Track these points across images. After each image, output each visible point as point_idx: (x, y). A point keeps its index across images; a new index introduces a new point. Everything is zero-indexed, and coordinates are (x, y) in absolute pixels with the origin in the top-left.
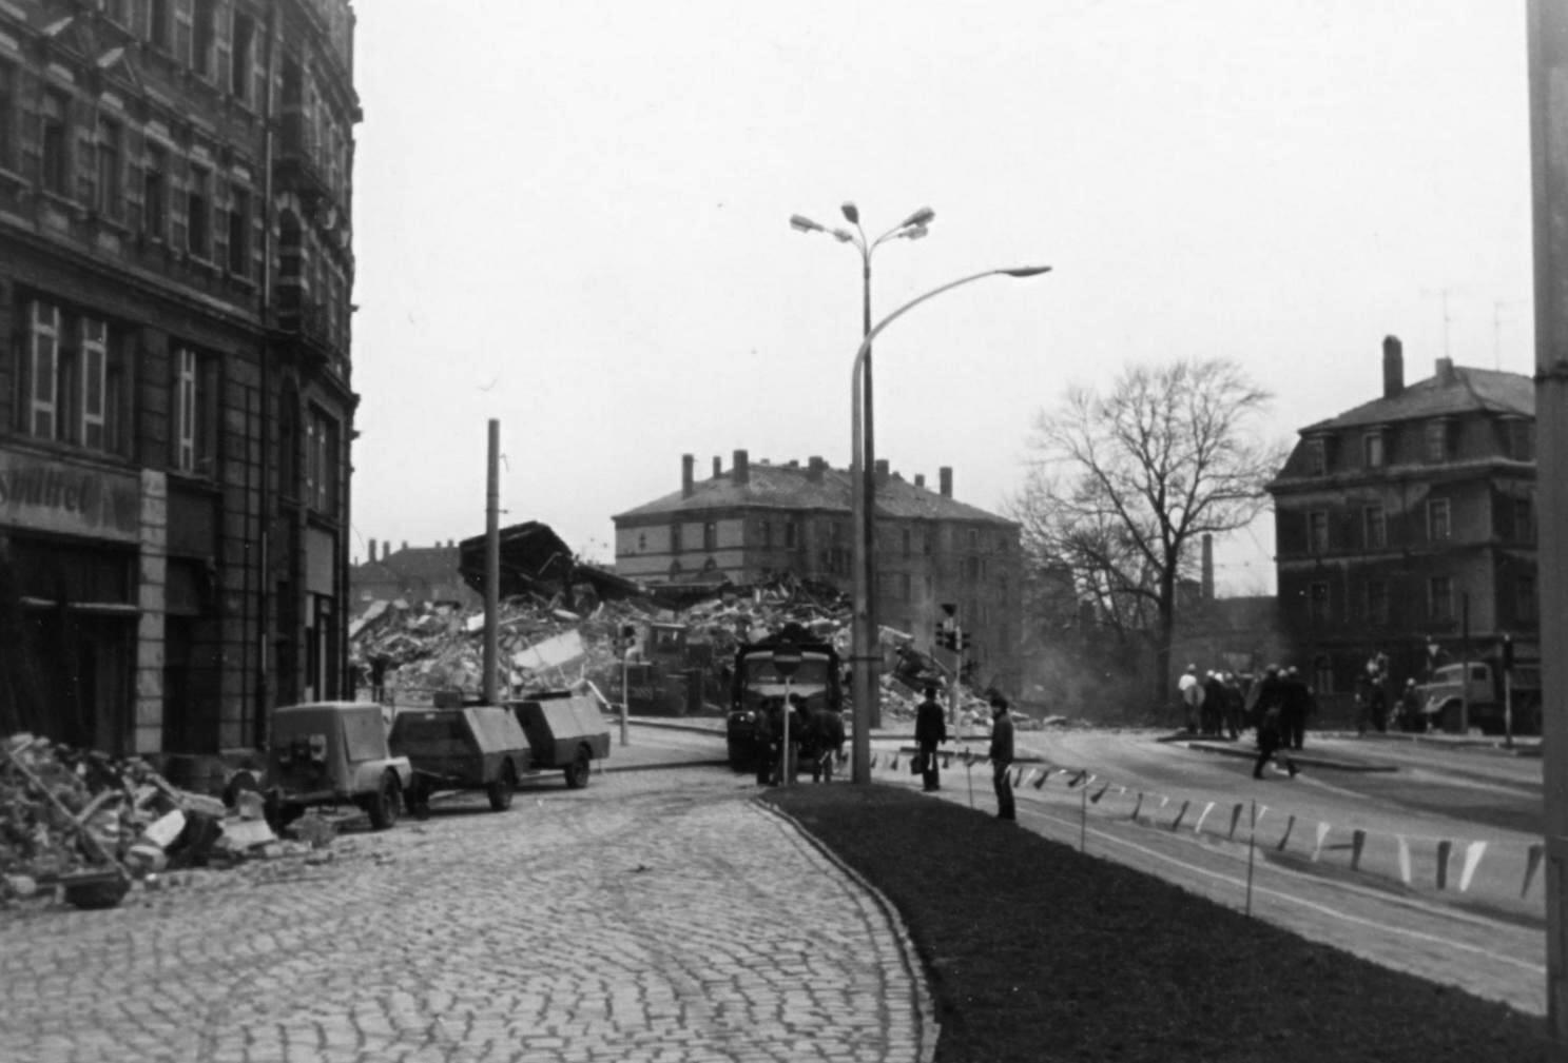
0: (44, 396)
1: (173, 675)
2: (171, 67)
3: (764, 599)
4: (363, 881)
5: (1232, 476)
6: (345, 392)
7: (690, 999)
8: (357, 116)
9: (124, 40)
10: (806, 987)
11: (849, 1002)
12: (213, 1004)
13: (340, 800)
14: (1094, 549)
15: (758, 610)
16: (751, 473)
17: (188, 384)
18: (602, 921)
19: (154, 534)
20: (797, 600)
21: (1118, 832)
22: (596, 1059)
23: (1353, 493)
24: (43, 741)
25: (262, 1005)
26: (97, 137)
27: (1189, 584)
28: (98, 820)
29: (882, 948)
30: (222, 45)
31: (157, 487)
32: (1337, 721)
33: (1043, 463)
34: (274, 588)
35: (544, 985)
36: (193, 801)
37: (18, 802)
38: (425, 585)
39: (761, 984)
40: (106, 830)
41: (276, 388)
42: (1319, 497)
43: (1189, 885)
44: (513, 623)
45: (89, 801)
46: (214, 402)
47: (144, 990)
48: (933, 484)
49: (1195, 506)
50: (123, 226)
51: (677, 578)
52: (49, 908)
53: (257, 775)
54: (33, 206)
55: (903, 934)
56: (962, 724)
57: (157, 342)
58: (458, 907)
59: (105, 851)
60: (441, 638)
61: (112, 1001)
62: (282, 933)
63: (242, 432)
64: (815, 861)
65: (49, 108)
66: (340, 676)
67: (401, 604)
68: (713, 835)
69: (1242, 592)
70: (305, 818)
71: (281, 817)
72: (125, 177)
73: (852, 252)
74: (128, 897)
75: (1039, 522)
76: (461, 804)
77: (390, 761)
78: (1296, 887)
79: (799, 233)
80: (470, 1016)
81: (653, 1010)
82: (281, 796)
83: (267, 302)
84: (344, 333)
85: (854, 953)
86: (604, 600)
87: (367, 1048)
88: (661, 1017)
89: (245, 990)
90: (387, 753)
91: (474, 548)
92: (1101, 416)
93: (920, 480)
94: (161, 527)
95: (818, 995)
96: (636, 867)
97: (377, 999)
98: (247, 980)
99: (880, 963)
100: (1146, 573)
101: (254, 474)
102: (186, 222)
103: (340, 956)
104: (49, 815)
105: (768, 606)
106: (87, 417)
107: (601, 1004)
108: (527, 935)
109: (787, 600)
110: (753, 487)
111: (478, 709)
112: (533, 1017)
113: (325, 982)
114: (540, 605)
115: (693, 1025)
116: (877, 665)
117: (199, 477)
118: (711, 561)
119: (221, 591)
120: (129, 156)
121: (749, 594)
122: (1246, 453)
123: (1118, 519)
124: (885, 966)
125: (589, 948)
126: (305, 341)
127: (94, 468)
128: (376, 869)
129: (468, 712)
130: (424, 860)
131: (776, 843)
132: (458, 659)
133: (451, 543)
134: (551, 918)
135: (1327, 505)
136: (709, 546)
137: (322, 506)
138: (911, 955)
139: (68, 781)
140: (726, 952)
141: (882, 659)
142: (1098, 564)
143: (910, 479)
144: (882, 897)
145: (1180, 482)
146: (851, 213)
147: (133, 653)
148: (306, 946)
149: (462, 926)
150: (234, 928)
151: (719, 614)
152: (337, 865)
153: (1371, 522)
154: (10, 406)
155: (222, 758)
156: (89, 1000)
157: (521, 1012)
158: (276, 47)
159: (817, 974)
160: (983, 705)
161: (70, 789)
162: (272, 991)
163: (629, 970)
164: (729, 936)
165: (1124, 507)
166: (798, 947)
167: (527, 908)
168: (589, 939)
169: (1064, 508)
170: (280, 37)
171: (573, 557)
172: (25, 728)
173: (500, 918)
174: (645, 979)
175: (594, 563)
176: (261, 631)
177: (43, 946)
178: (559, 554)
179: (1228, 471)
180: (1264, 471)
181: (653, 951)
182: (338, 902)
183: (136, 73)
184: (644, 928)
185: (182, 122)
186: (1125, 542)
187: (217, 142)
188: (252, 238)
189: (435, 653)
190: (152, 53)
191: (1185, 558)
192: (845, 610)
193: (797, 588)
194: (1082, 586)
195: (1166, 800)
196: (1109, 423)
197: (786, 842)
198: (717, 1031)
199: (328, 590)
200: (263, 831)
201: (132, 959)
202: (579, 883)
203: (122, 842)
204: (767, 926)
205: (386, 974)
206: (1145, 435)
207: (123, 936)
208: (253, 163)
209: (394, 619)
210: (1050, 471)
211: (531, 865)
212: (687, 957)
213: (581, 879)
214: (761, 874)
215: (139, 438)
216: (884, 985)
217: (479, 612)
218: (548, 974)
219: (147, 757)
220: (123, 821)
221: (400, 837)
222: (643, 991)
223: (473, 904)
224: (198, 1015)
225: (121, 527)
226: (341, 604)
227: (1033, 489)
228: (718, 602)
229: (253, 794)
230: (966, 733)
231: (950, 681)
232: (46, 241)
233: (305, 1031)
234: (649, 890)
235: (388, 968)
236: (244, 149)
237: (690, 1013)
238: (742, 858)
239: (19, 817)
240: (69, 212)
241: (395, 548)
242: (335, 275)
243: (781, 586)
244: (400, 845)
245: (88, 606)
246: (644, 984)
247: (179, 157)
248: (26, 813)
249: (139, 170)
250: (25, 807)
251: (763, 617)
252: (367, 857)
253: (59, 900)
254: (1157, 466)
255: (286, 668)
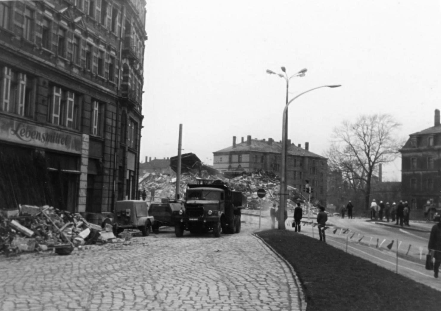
0: (56, 113)
1: (89, 191)
2: (94, 22)
3: (255, 176)
4: (139, 250)
5: (389, 147)
6: (140, 115)
7: (232, 290)
8: (146, 38)
9: (81, 14)
10: (266, 289)
11: (279, 294)
12: (93, 285)
13: (134, 227)
14: (349, 166)
15: (253, 180)
16: (252, 142)
17: (96, 111)
18: (207, 266)
19: (85, 151)
20: (264, 177)
21: (355, 246)
22: (204, 308)
23: (424, 153)
24: (52, 208)
25: (108, 285)
26: (74, 41)
27: (375, 177)
28: (66, 230)
29: (288, 278)
30: (109, 17)
31: (86, 139)
32: (418, 218)
33: (335, 142)
34: (118, 168)
35: (189, 284)
36: (93, 226)
37: (44, 224)
38: (161, 169)
39: (253, 287)
40: (68, 233)
41: (120, 113)
42: (415, 154)
43: (379, 264)
44: (184, 181)
45: (64, 225)
46: (103, 116)
47: (75, 280)
48: (303, 147)
49: (378, 155)
50: (80, 66)
51: (230, 170)
52: (51, 255)
53: (111, 219)
54: (55, 60)
55: (295, 274)
56: (310, 214)
57: (88, 99)
58: (165, 260)
59: (68, 239)
60: (164, 184)
61: (65, 282)
62: (115, 265)
63: (111, 125)
64: (268, 251)
65: (60, 33)
66: (136, 193)
67: (154, 174)
68: (239, 242)
69: (391, 180)
70: (124, 232)
71: (117, 232)
72: (81, 52)
73: (283, 80)
74: (73, 252)
75: (333, 158)
76: (168, 230)
77: (148, 217)
78: (410, 266)
79: (268, 75)
80: (167, 292)
81: (221, 293)
82: (118, 226)
83: (119, 89)
84: (140, 98)
85: (280, 279)
86: (210, 175)
87: (137, 301)
88: (223, 296)
89: (103, 281)
90: (148, 215)
91: (174, 159)
92: (352, 129)
93: (299, 145)
94: (87, 150)
95: (270, 291)
96: (217, 250)
97: (141, 285)
98: (104, 278)
99: (288, 282)
100: (363, 174)
101: (114, 136)
102: (97, 66)
103: (131, 272)
104: (52, 229)
105: (256, 178)
106: (68, 119)
107: (206, 291)
108: (185, 269)
109: (261, 177)
110: (253, 146)
111: (173, 204)
112: (186, 293)
113: (126, 280)
114: (192, 176)
115: (232, 299)
116: (287, 196)
117: (98, 136)
118: (240, 166)
119: (103, 168)
120: (82, 47)
121: (250, 175)
122: (394, 141)
123: (356, 158)
124: (290, 284)
125: (203, 273)
126: (129, 100)
127: (70, 133)
128: (143, 247)
129: (171, 204)
130: (157, 245)
131: (257, 245)
132: (169, 190)
133: (168, 158)
134: (192, 264)
135: (417, 156)
136: (240, 162)
137: (132, 146)
138: (297, 281)
139: (58, 219)
140: (243, 277)
141: (288, 195)
142: (349, 170)
143: (297, 145)
144: (288, 263)
145: (374, 148)
146: (284, 69)
147: (79, 184)
148: (122, 269)
149: (167, 265)
150: (102, 263)
151: (242, 180)
152: (132, 246)
153: (429, 161)
154: (47, 115)
155: (102, 214)
156: (58, 282)
157: (182, 292)
158: (124, 19)
159: (269, 285)
160: (316, 209)
161: (59, 221)
162: (111, 282)
163: (214, 281)
164: (243, 272)
165: (358, 155)
166: (264, 276)
167: (185, 261)
168: (203, 271)
169: (341, 154)
170: (125, 15)
171: (202, 163)
172: (47, 204)
173: (177, 264)
174: (218, 284)
175: (207, 165)
176: (114, 180)
177: (47, 265)
178: (197, 162)
179: (388, 146)
180: (399, 146)
181: (221, 275)
182: (131, 256)
183: (84, 24)
184: (219, 269)
185: (97, 38)
186: (358, 165)
187: (106, 44)
188: (115, 71)
189: (162, 188)
190: (89, 18)
191: (375, 170)
192: (278, 180)
193: (264, 174)
194: (345, 176)
195: (372, 238)
196: (354, 131)
197: (260, 245)
198: (240, 302)
199: (133, 169)
200: (112, 235)
201: (72, 270)
202: (200, 254)
203: (72, 237)
204: (255, 270)
205: (144, 278)
206: (365, 135)
207: (70, 263)
208: (117, 50)
209: (151, 178)
210: (337, 144)
211: (187, 248)
212: (230, 277)
213: (201, 253)
214: (253, 254)
215: (82, 125)
216: (290, 289)
217: (175, 177)
218: (190, 281)
219: (81, 213)
220: (73, 231)
221: (150, 240)
222: (218, 287)
223: (170, 259)
224: (89, 288)
225: (76, 150)
226: (136, 173)
227: (332, 149)
228: (242, 177)
229: (109, 225)
230: (311, 216)
231: (306, 202)
232: (58, 70)
233: (119, 294)
234: (221, 257)
235: (145, 277)
236: (114, 46)
237: (232, 295)
238: (247, 249)
239: (44, 229)
240: (65, 62)
241: (153, 159)
242: (138, 82)
243: (259, 173)
244: (150, 241)
245: (66, 171)
246: (218, 285)
247: (95, 47)
248: (46, 228)
249: (84, 51)
250: (46, 226)
251: (254, 182)
252: (141, 244)
253: (54, 252)
254: (368, 143)
255: (121, 190)
